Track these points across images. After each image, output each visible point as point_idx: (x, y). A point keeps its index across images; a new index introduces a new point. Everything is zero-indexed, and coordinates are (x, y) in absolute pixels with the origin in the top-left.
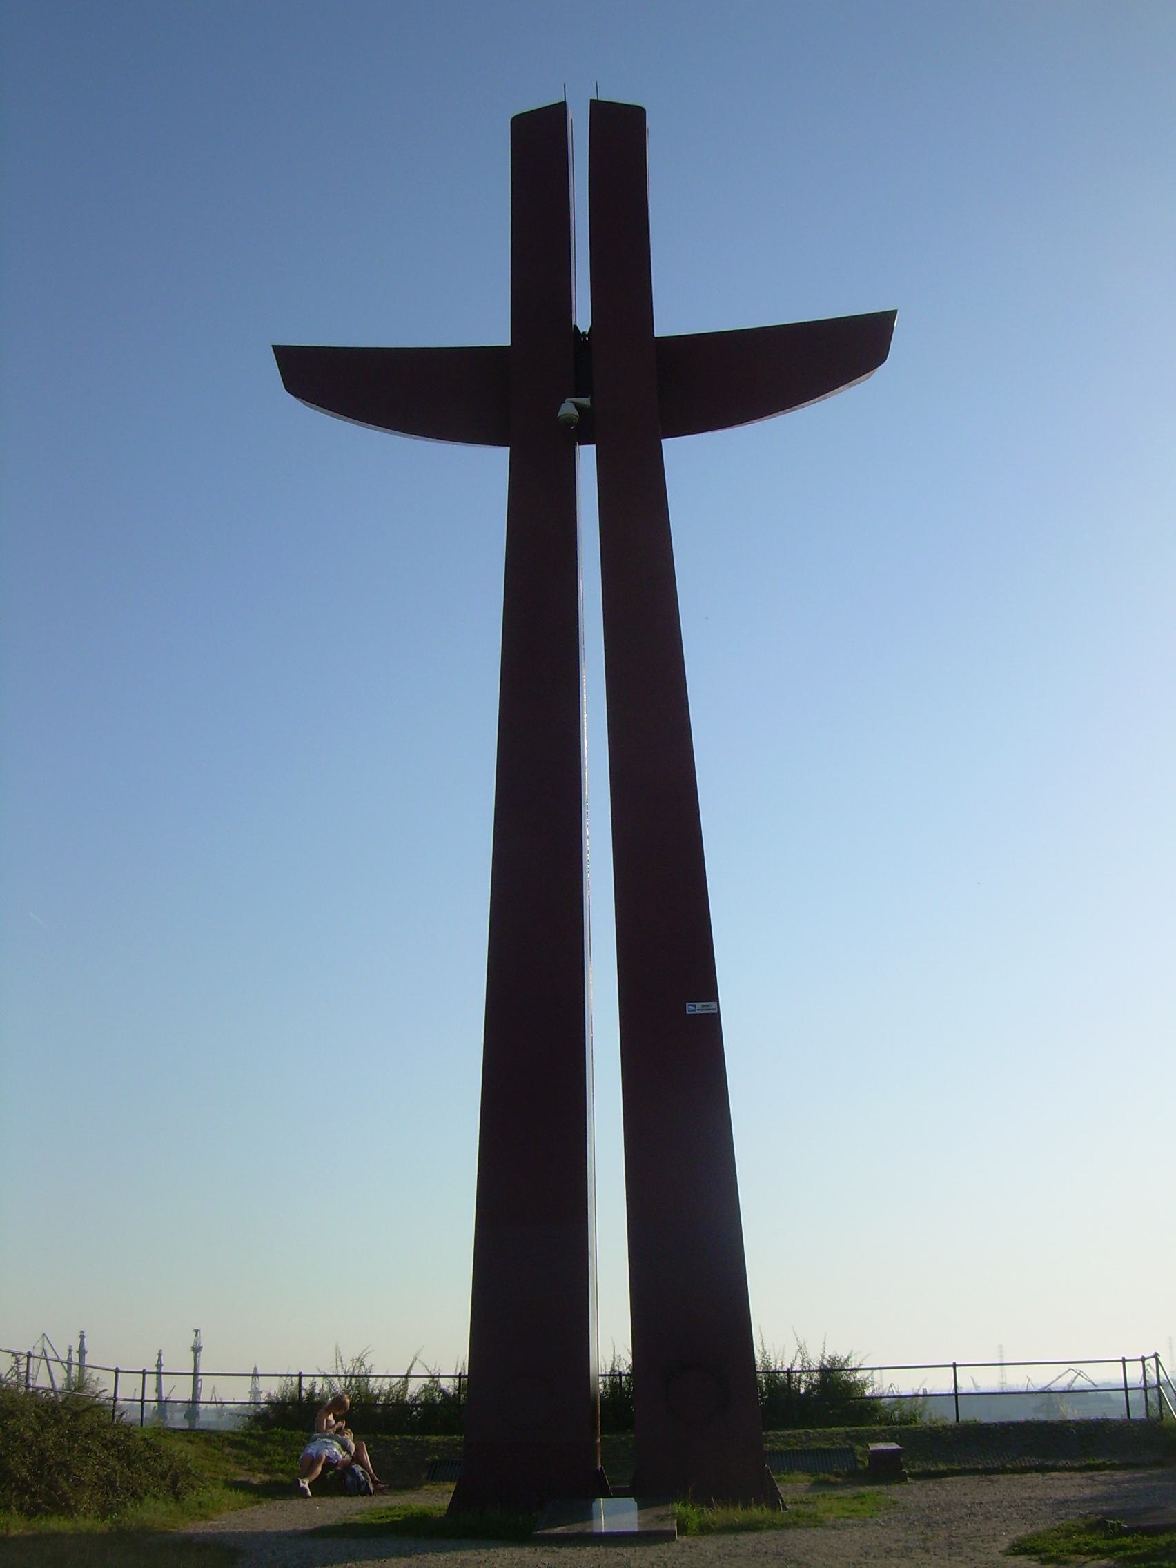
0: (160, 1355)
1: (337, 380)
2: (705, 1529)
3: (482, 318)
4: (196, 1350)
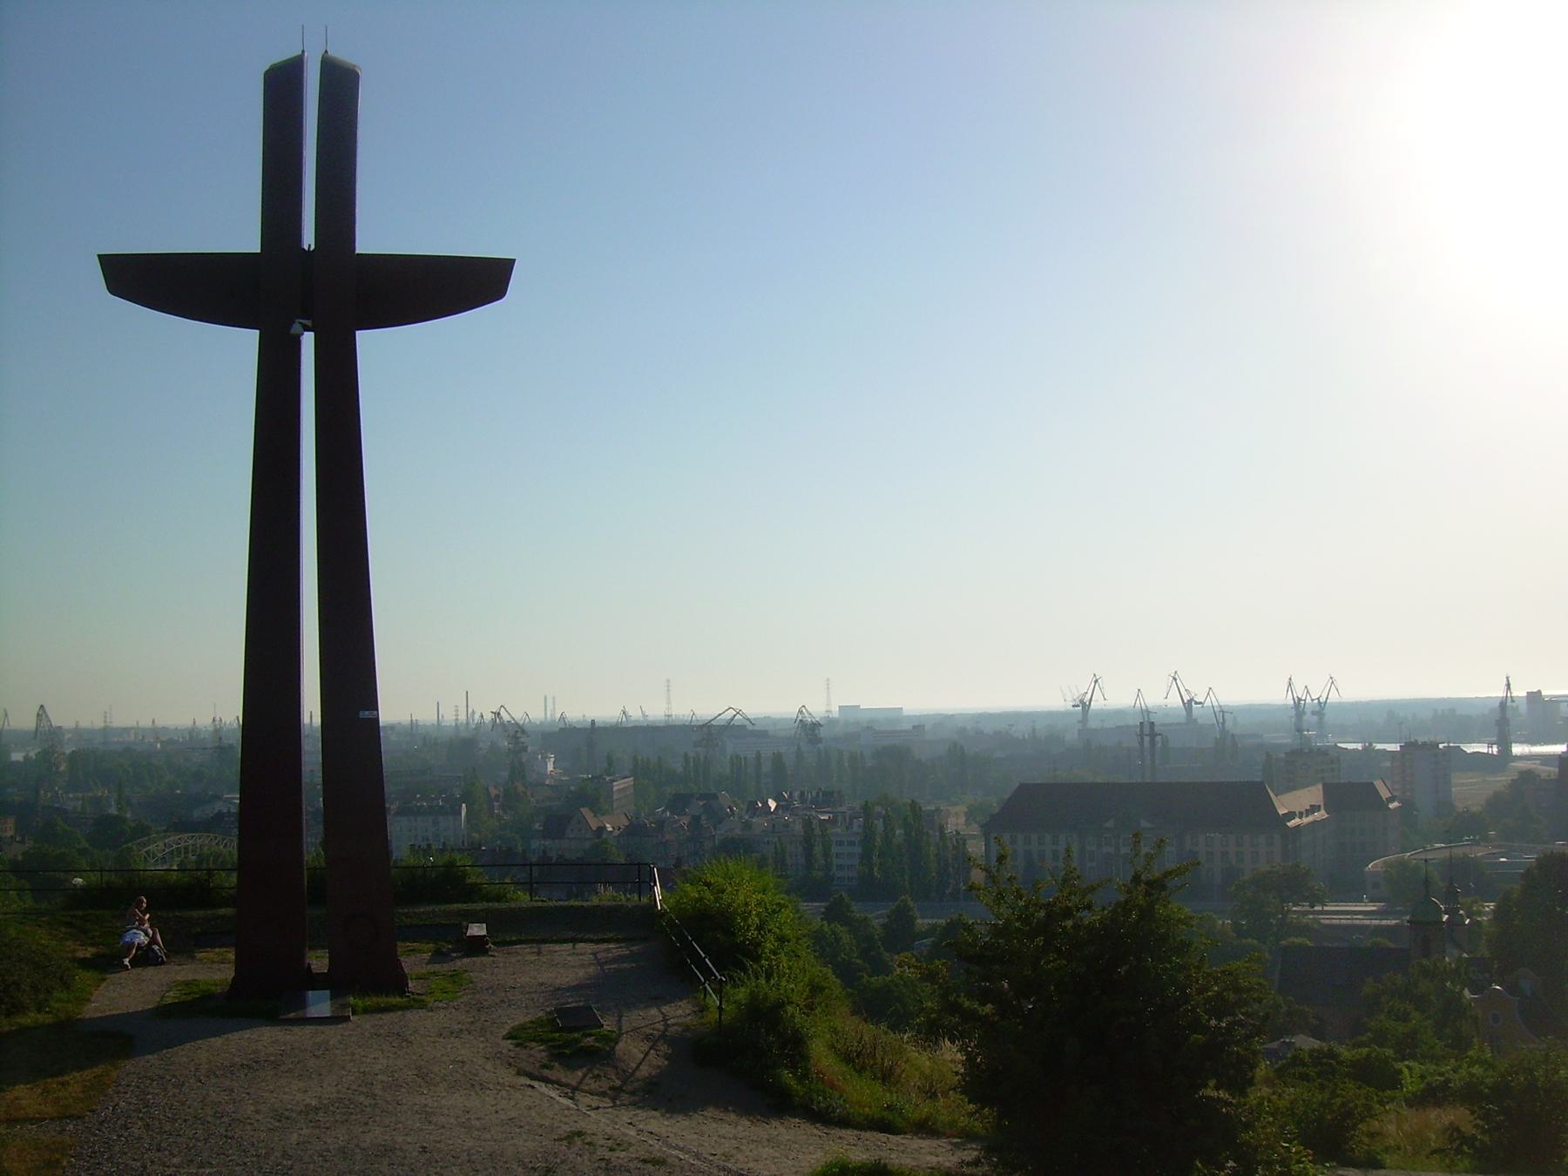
2: (366, 1011)
3: (236, 229)
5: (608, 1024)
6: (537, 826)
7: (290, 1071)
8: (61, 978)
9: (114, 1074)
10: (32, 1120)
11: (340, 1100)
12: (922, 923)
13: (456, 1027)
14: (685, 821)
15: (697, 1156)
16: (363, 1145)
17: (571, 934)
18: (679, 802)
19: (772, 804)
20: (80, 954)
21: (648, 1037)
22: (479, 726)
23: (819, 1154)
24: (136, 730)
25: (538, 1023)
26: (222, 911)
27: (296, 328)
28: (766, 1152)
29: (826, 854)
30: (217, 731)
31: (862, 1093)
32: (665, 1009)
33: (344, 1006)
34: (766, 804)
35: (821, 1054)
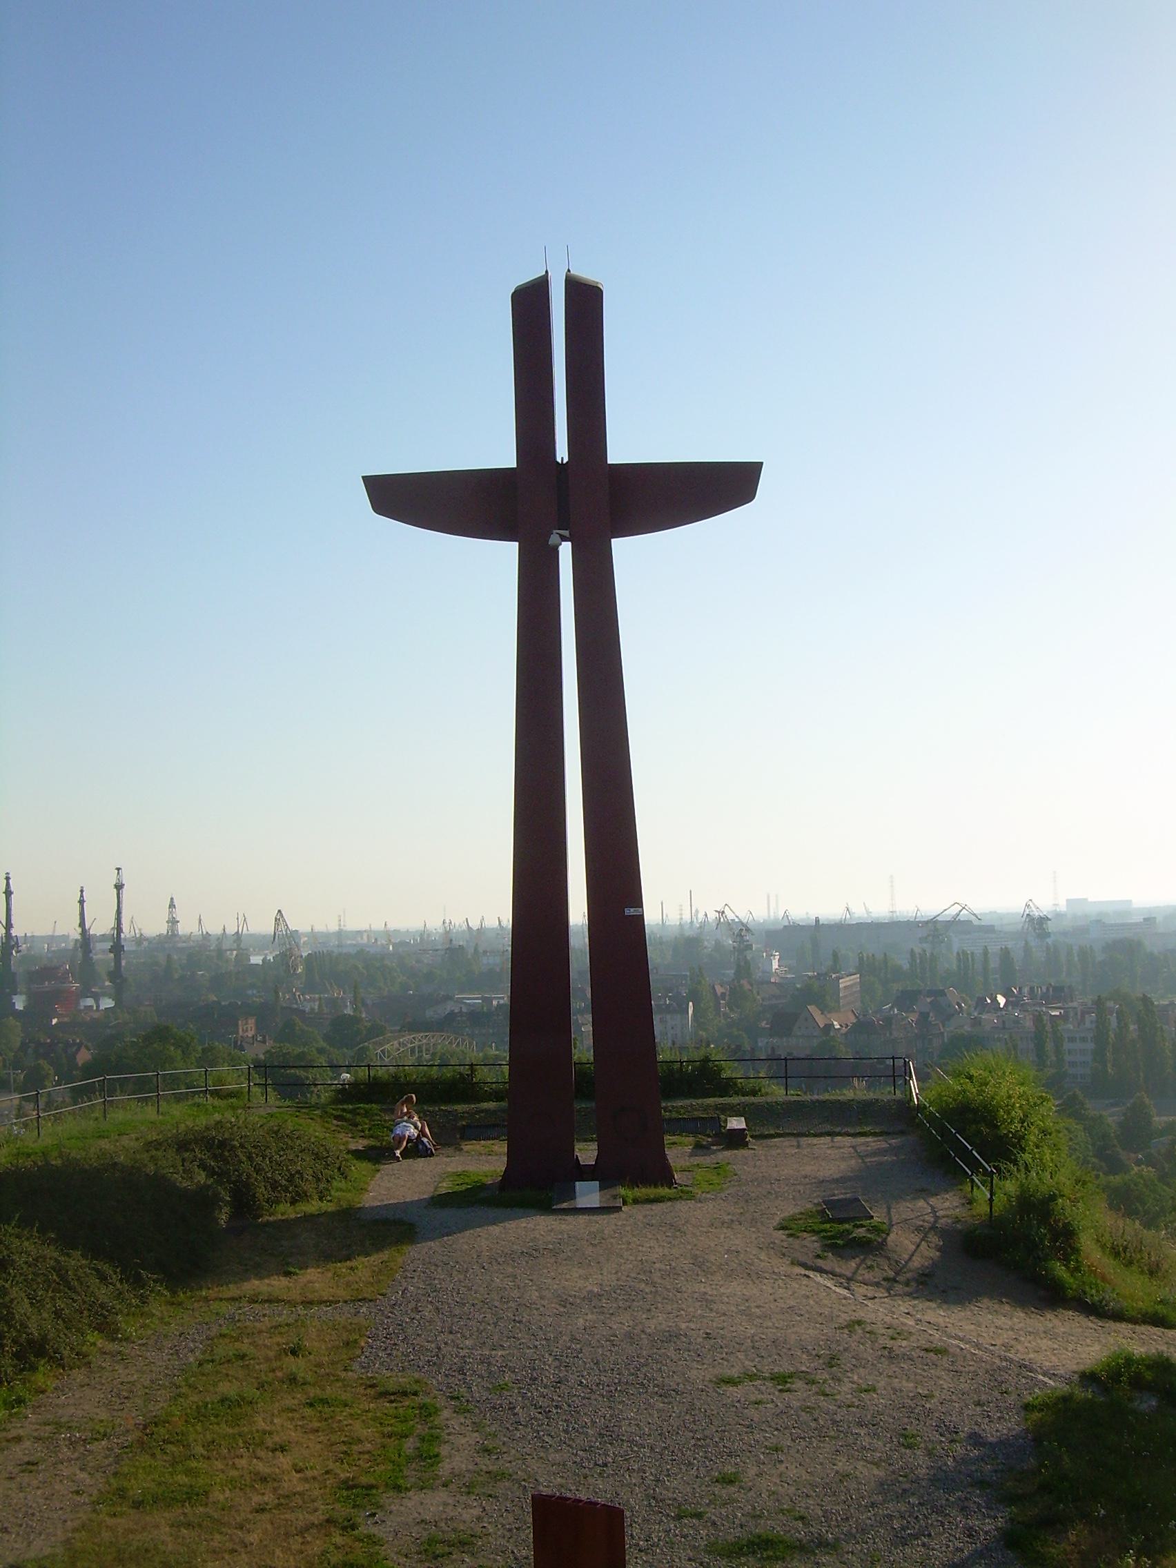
0: (82, 891)
1: (402, 497)
2: (636, 1201)
4: (119, 887)
5: (878, 1217)
6: (763, 1024)
7: (569, 1258)
8: (339, 1169)
9: (400, 1260)
10: (328, 1303)
11: (622, 1288)
12: (1159, 1121)
13: (727, 1218)
14: (913, 1018)
15: (977, 1346)
16: (648, 1331)
17: (828, 1128)
18: (906, 999)
19: (1001, 1000)
20: (353, 1147)
21: (918, 1229)
22: (703, 925)
23: (1097, 1347)
24: (369, 932)
25: (808, 1215)
26: (485, 1105)
27: (554, 539)
28: (1045, 1343)
29: (1058, 1051)
30: (447, 933)
31: (1132, 1288)
32: (933, 1201)
33: (615, 1197)
34: (994, 1000)
35: (1090, 1249)
